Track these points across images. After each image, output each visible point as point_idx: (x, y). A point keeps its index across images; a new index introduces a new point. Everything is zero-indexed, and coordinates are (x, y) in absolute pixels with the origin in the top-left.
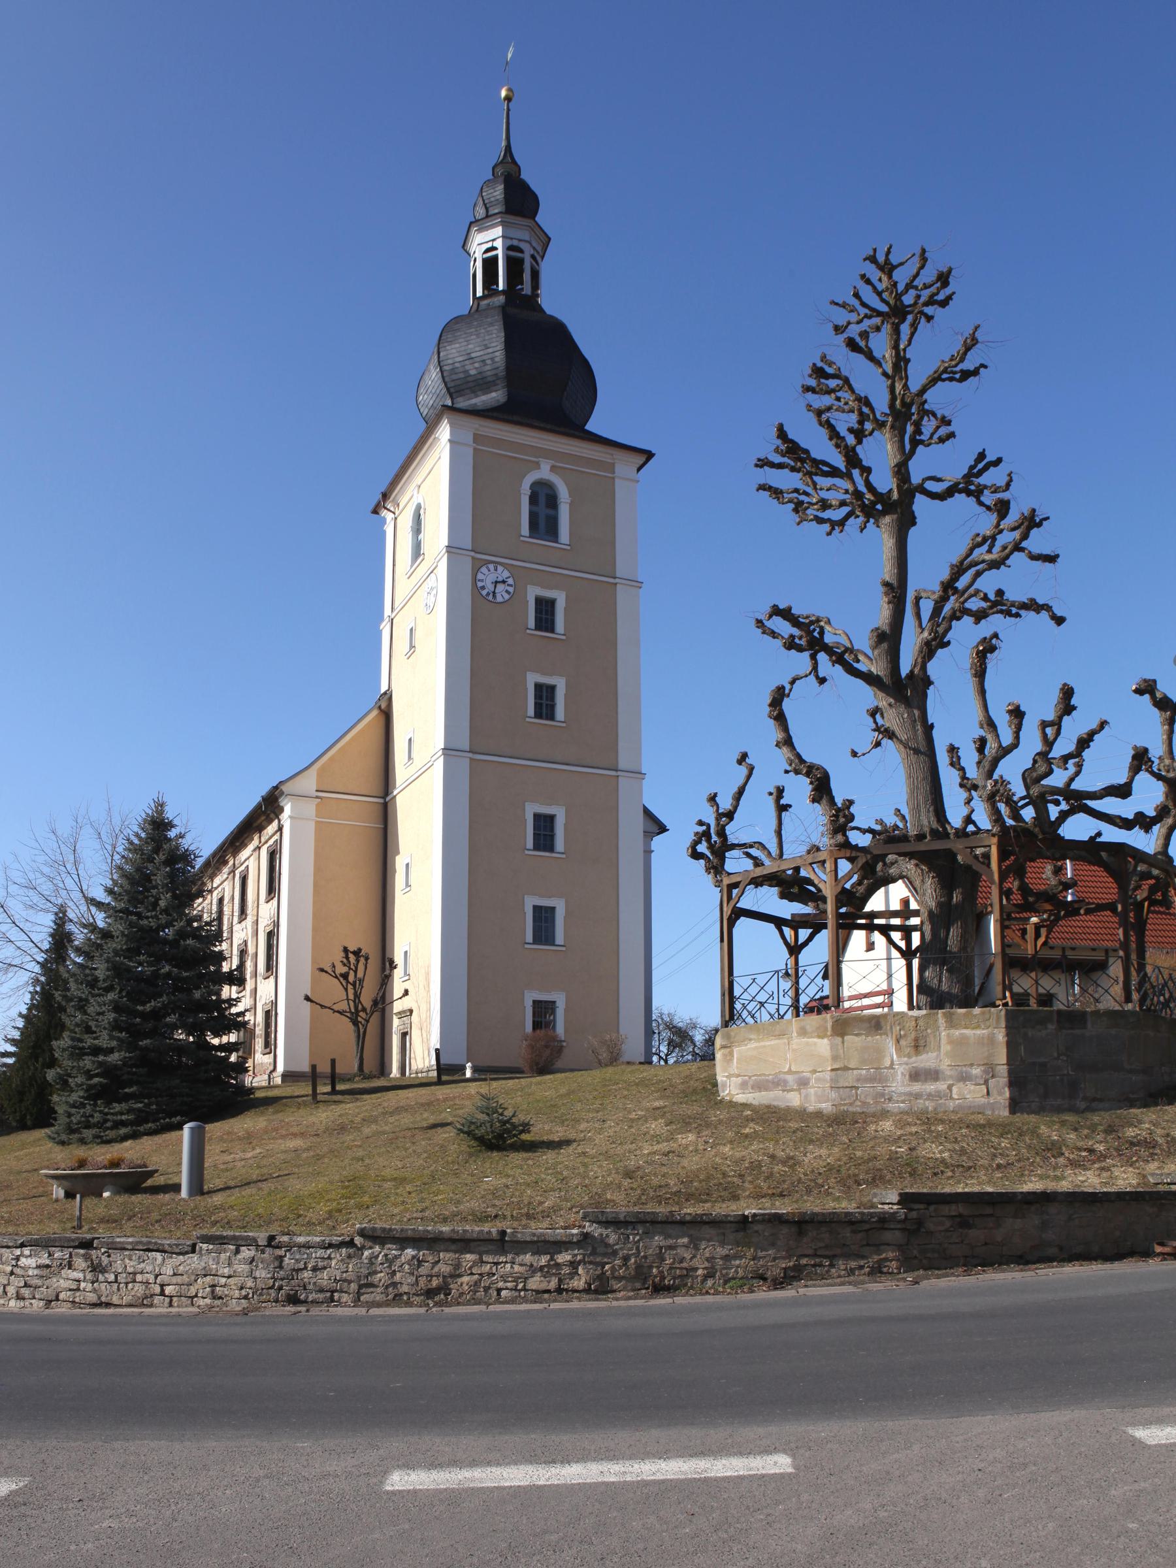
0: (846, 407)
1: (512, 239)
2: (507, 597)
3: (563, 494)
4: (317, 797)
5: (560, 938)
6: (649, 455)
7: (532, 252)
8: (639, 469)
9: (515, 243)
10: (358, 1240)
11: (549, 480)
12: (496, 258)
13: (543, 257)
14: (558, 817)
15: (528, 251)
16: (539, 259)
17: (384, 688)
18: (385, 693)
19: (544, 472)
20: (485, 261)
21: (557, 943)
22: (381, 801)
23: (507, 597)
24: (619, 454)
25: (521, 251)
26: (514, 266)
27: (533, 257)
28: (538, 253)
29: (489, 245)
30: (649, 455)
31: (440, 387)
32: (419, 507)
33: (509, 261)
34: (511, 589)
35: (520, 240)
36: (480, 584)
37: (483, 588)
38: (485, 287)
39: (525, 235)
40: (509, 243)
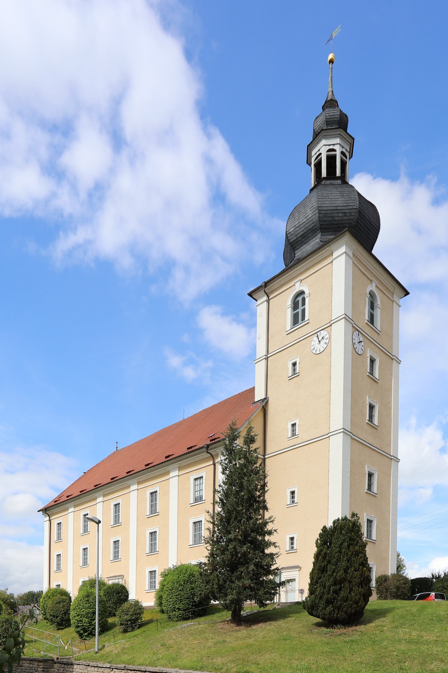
6: (407, 293)
12: (335, 157)
29: (331, 147)
30: (407, 293)
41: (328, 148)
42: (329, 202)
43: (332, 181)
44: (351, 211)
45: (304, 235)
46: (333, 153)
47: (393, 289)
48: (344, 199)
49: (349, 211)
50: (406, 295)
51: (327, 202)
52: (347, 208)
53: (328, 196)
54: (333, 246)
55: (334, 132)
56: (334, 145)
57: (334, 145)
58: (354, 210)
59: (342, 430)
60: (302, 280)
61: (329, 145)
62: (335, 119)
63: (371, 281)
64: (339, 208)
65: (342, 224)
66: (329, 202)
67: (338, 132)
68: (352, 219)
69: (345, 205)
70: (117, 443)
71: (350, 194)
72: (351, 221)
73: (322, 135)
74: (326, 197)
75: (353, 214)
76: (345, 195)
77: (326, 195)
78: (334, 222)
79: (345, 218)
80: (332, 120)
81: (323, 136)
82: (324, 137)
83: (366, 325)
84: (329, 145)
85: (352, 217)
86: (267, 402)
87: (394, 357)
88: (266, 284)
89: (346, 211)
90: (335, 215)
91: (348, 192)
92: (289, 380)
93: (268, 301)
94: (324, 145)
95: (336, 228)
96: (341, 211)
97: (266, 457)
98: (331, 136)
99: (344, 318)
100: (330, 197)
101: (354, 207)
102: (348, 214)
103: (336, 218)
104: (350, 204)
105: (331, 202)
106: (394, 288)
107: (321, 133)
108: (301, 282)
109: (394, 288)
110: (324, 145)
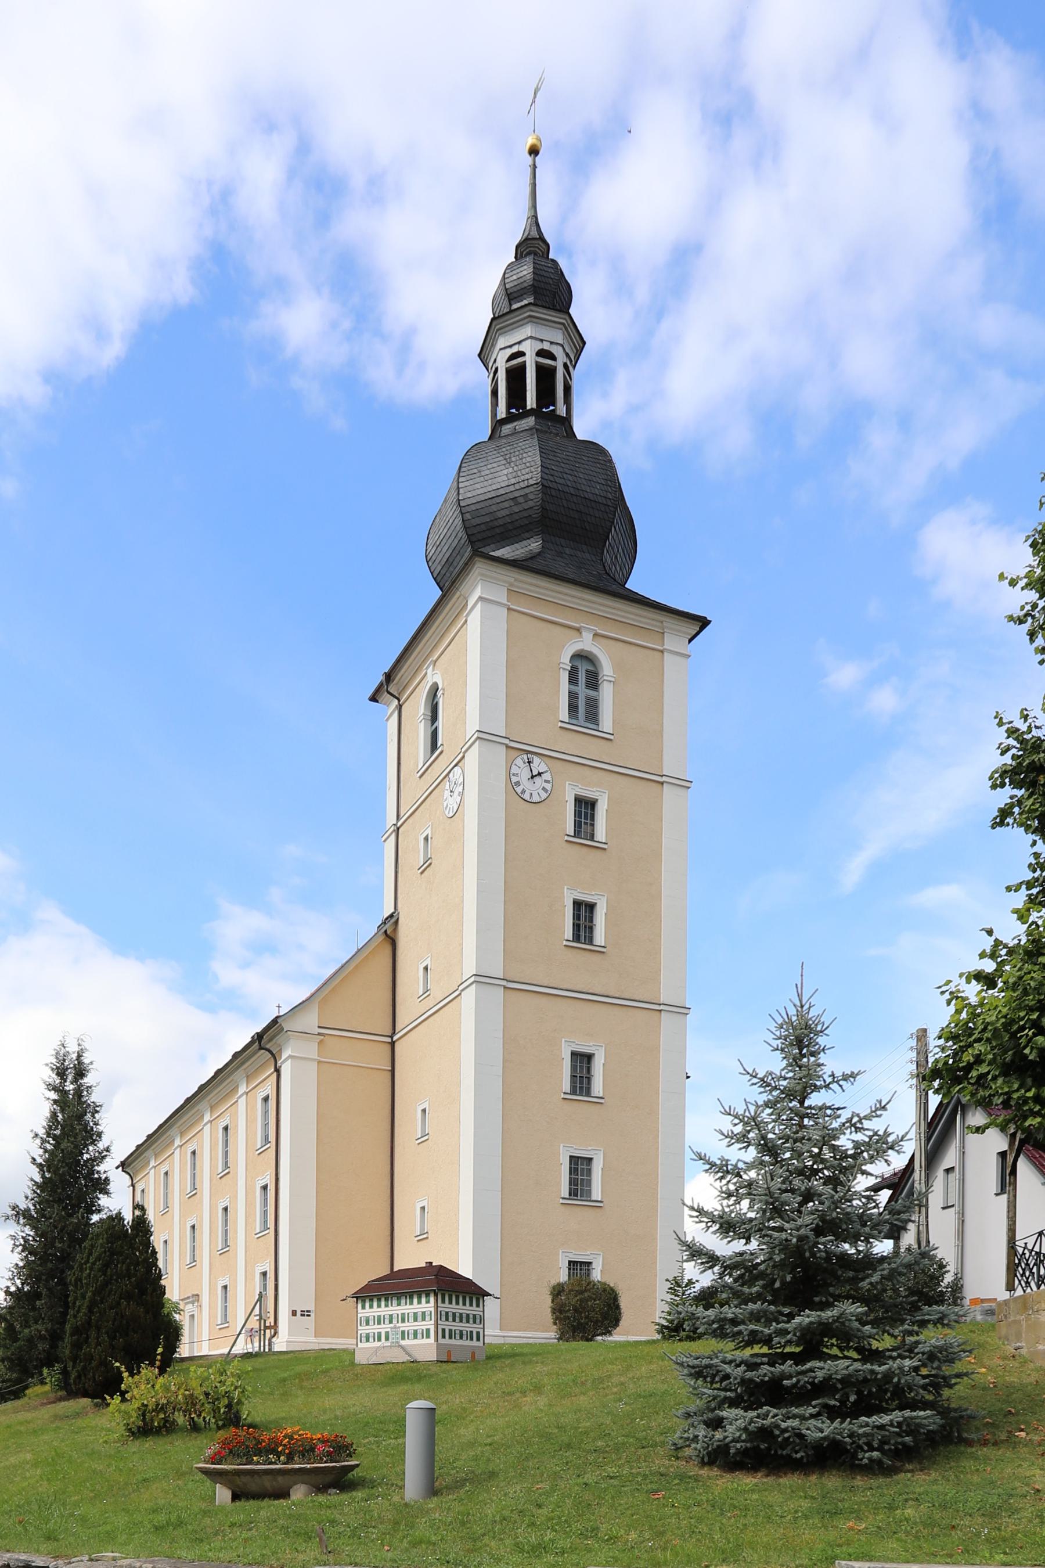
0: (538, 765)
1: (542, 341)
2: (544, 795)
3: (607, 669)
4: (319, 1034)
5: (596, 1193)
6: (703, 623)
7: (565, 360)
8: (690, 641)
9: (546, 346)
10: (866, 1448)
11: (590, 652)
12: (522, 367)
13: (574, 367)
14: (596, 1056)
15: (561, 359)
16: (571, 369)
17: (388, 910)
18: (391, 916)
19: (586, 643)
20: (509, 372)
21: (593, 1198)
22: (389, 1040)
23: (544, 795)
24: (669, 622)
25: (553, 358)
26: (545, 375)
27: (565, 366)
28: (571, 361)
29: (515, 349)
30: (703, 623)
31: (460, 535)
32: (435, 690)
33: (540, 369)
34: (548, 786)
35: (552, 343)
36: (514, 779)
37: (518, 784)
38: (509, 406)
39: (558, 337)
40: (539, 346)
41: (509, 352)
42: (482, 485)
43: (515, 424)
44: (527, 491)
45: (451, 560)
46: (520, 360)
47: (659, 624)
48: (511, 470)
49: (522, 493)
50: (702, 629)
51: (477, 486)
52: (517, 487)
53: (480, 472)
54: (464, 588)
55: (518, 316)
56: (519, 343)
57: (519, 343)
58: (531, 489)
59: (472, 979)
60: (436, 662)
61: (510, 346)
62: (525, 285)
63: (578, 630)
64: (502, 492)
65: (512, 522)
66: (482, 485)
67: (525, 312)
68: (531, 508)
69: (513, 481)
70: (279, 1007)
71: (525, 455)
72: (530, 512)
73: (528, 314)
74: (475, 476)
75: (531, 497)
76: (513, 459)
77: (475, 471)
78: (496, 523)
79: (516, 509)
80: (518, 288)
81: (498, 330)
82: (500, 332)
83: (562, 732)
84: (510, 346)
85: (531, 504)
86: (397, 922)
87: (664, 779)
88: (389, 677)
89: (517, 494)
90: (494, 508)
91: (521, 452)
92: (422, 873)
93: (400, 707)
94: (501, 349)
95: (502, 533)
96: (506, 497)
97: (395, 1038)
98: (514, 326)
99: (478, 738)
100: (483, 474)
101: (531, 482)
102: (521, 500)
103: (500, 514)
104: (522, 478)
105: (486, 483)
106: (662, 622)
107: (493, 326)
108: (434, 666)
109: (662, 622)
110: (501, 349)
